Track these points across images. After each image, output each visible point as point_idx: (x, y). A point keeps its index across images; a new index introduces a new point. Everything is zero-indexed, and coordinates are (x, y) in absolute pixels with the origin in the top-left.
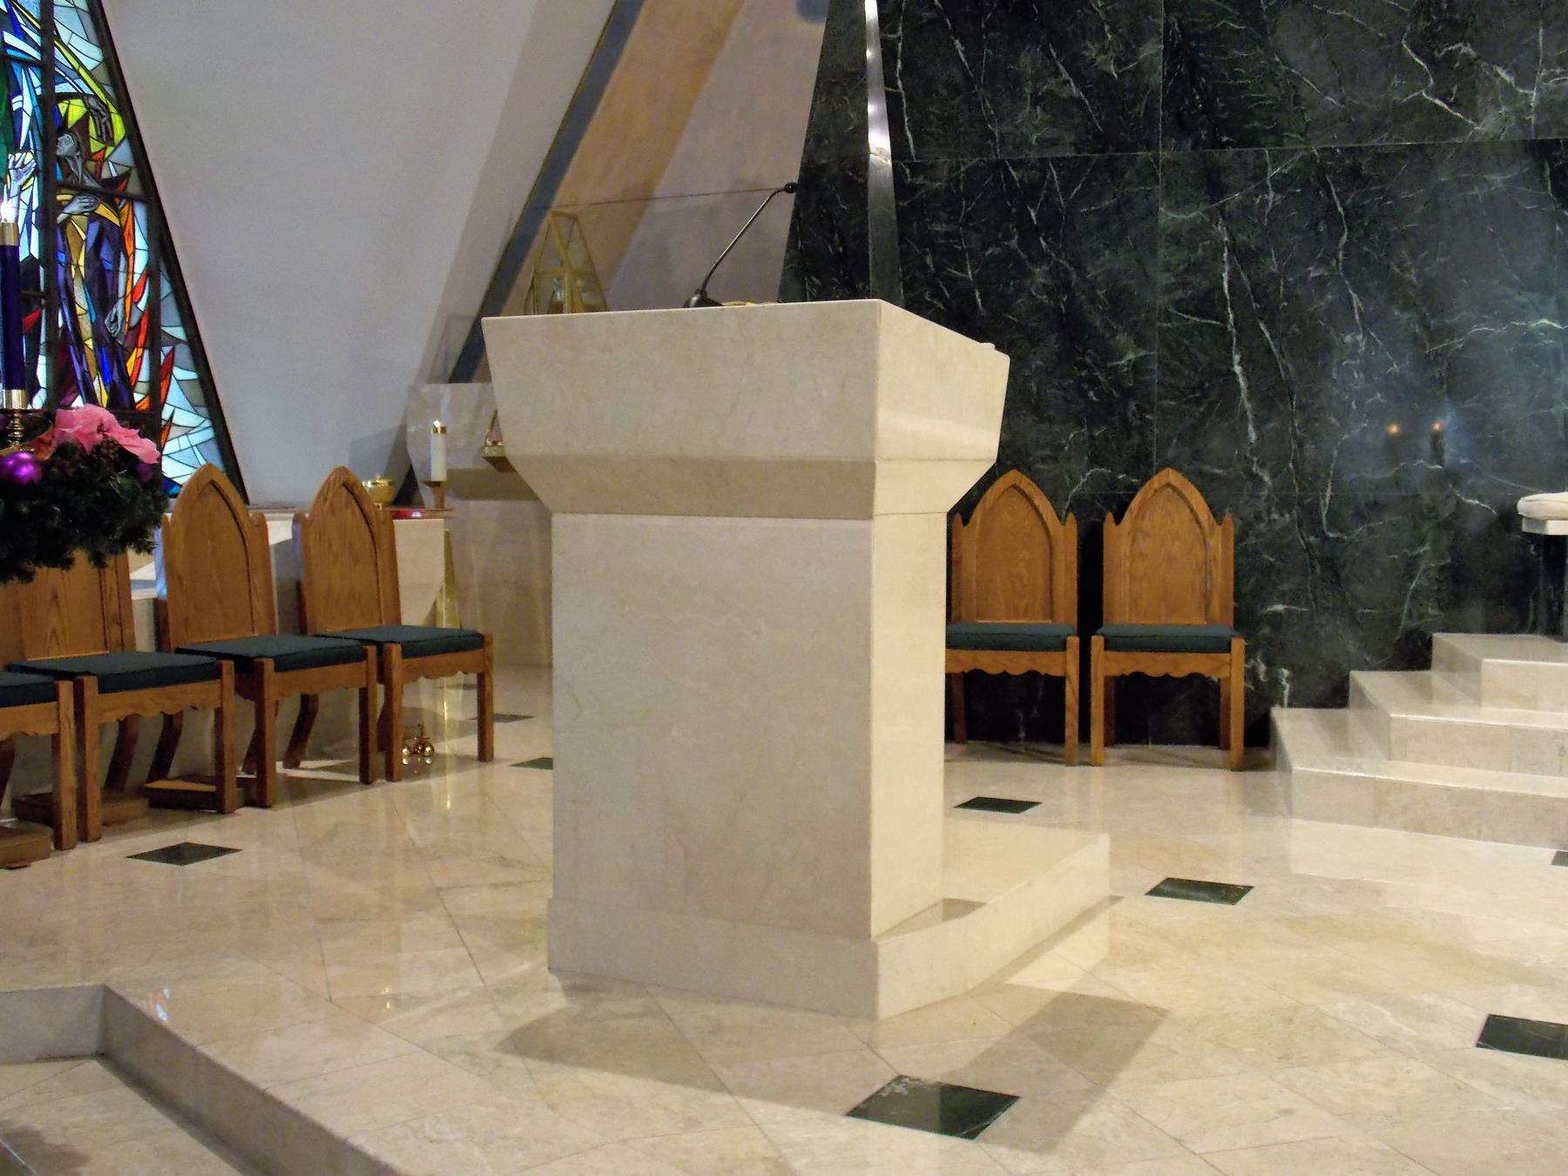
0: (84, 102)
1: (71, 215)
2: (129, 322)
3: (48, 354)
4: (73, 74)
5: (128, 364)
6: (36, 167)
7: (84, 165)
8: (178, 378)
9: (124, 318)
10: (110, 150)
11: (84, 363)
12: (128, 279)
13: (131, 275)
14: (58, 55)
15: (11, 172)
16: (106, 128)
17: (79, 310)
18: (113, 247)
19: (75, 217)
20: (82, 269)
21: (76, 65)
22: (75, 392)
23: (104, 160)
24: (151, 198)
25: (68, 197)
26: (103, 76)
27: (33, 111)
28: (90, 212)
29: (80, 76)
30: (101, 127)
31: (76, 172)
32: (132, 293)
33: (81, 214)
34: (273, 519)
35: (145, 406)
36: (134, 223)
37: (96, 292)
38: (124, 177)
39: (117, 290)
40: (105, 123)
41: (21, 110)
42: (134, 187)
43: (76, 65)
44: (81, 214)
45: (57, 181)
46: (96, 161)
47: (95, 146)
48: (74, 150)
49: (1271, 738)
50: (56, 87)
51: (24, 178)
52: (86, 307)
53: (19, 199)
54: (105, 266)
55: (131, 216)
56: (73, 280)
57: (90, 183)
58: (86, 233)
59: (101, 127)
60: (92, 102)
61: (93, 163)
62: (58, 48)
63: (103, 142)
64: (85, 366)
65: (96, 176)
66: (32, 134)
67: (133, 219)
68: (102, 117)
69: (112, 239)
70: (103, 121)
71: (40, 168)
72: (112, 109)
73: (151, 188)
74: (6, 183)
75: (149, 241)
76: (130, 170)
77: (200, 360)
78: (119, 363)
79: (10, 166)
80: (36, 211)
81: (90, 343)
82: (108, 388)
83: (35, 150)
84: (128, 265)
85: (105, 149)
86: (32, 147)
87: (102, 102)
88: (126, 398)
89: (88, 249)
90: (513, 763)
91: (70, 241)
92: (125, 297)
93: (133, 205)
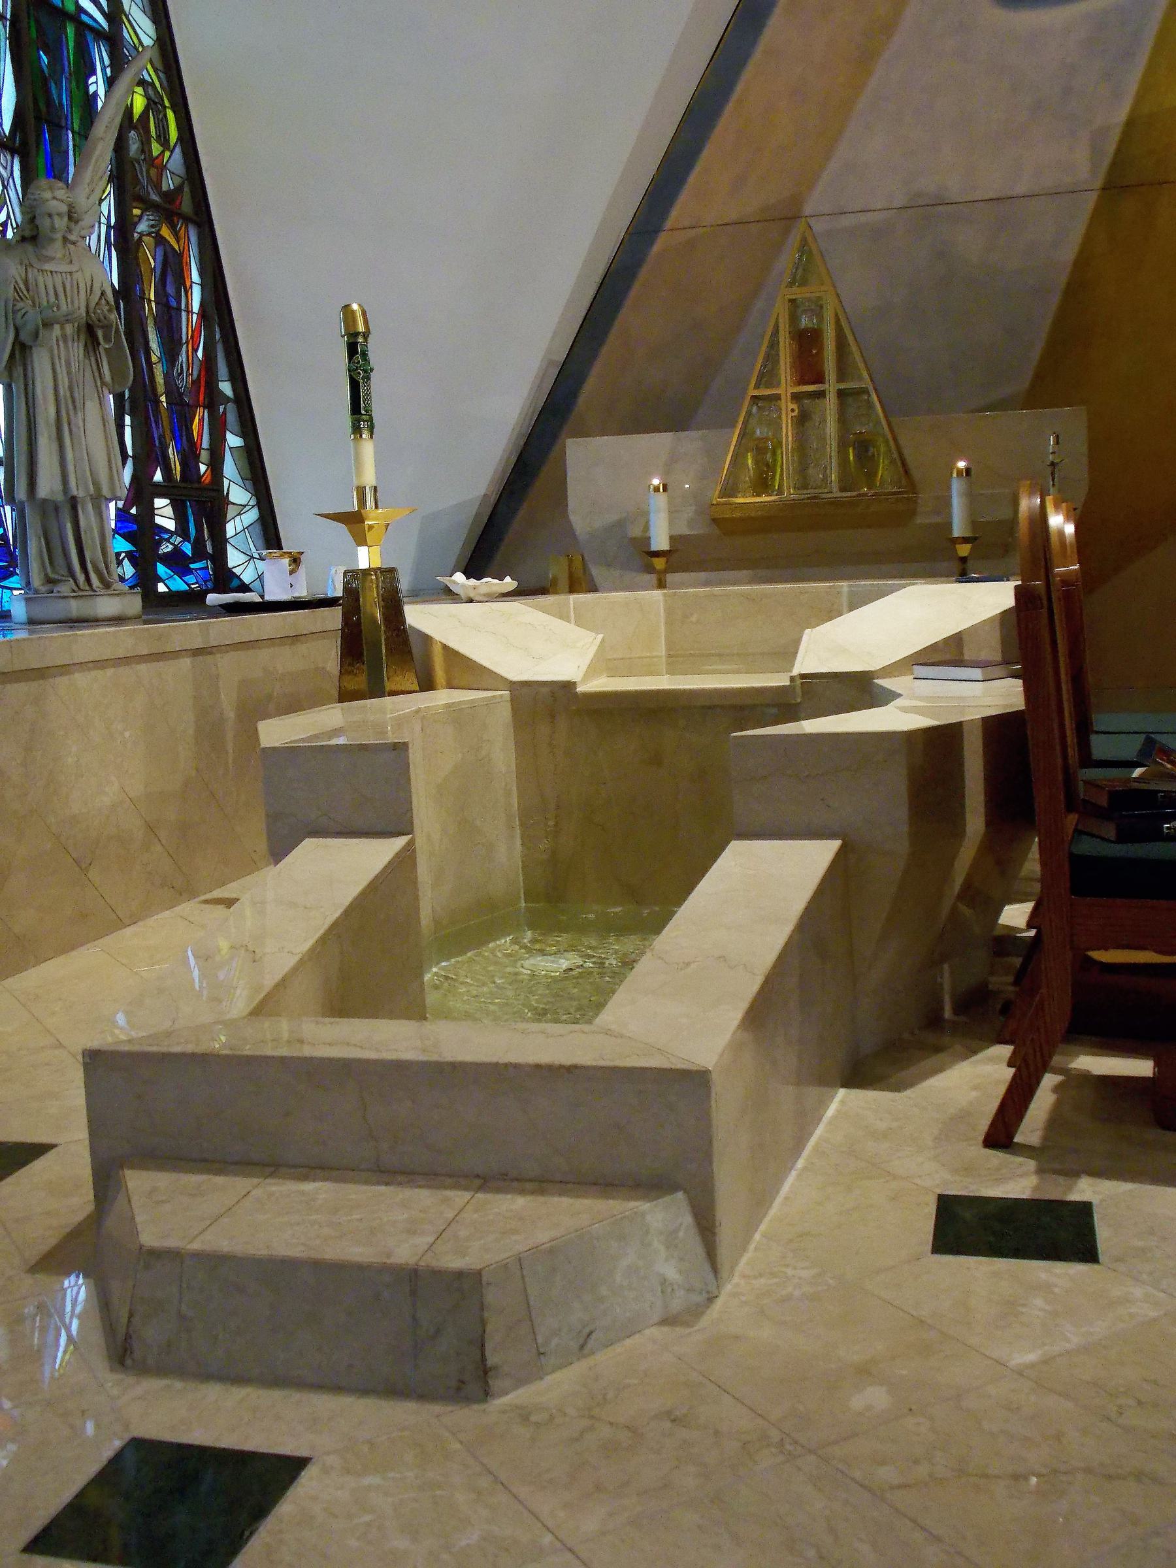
2: (192, 375)
8: (232, 445)
10: (167, 154)
16: (163, 127)
17: (154, 359)
24: (203, 219)
31: (142, 181)
32: (192, 337)
33: (149, 234)
34: (409, 603)
35: (207, 479)
38: (179, 189)
41: (96, 94)
42: (186, 206)
44: (149, 234)
47: (156, 149)
49: (1096, 1050)
52: (158, 355)
55: (186, 239)
64: (161, 430)
69: (173, 267)
73: (248, 416)
75: (201, 274)
77: (249, 429)
82: (180, 456)
90: (711, 1276)
92: (187, 342)
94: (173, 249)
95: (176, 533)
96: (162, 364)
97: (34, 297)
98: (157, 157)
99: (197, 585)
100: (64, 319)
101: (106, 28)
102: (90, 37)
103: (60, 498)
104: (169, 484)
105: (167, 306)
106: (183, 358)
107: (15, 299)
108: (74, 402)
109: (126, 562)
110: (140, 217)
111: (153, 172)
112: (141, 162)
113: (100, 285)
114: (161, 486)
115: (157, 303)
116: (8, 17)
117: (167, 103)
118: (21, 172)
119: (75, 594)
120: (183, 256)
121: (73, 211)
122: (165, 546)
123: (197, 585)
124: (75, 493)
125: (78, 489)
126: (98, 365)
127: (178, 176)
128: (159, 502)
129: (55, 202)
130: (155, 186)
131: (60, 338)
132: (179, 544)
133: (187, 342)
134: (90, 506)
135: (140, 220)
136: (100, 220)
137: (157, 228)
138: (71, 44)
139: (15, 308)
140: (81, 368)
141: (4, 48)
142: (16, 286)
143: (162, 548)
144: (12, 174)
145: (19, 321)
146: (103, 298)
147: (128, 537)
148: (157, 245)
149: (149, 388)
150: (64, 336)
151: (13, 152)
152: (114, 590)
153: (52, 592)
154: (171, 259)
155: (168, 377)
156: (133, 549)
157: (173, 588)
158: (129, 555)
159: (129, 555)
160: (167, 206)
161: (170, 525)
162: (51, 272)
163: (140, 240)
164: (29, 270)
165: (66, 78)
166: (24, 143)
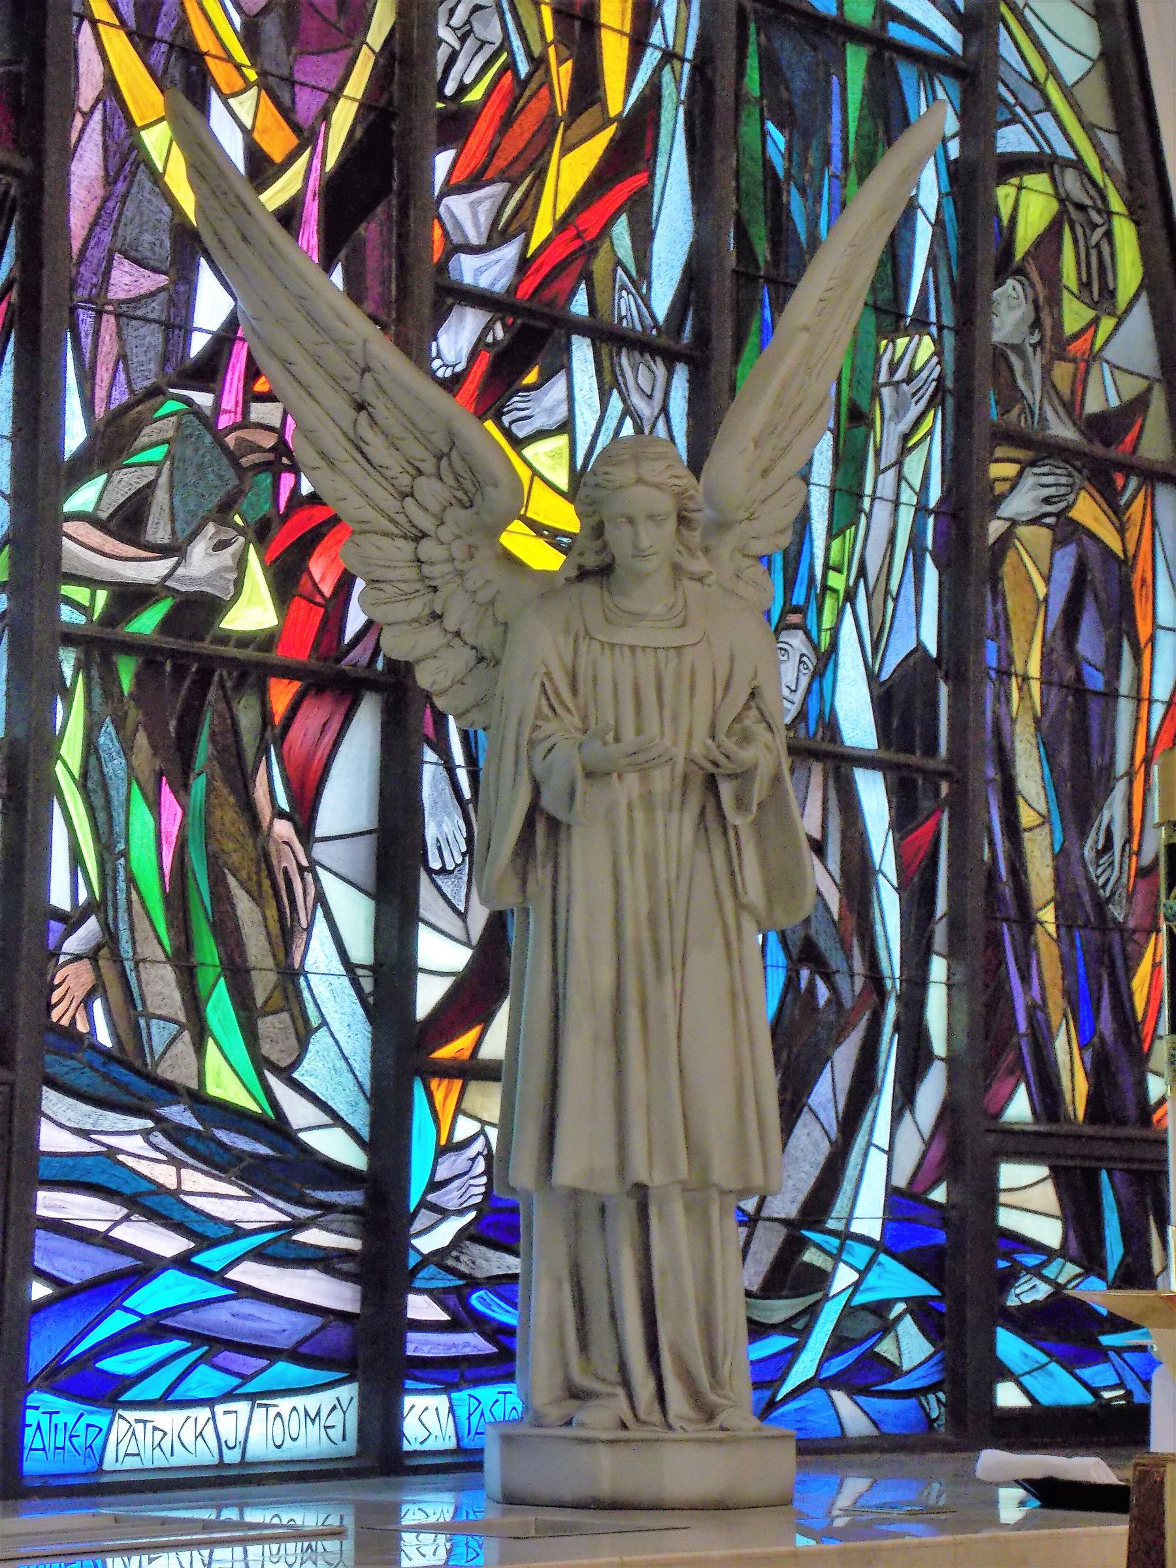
0: (1053, 179)
1: (1014, 523)
3: (952, 955)
4: (1033, 99)
5: (1136, 983)
6: (940, 379)
7: (1047, 370)
9: (1128, 841)
10: (1107, 324)
11: (1034, 972)
12: (1137, 719)
13: (1145, 705)
14: (1006, 48)
15: (886, 392)
17: (1027, 817)
18: (1105, 621)
19: (1022, 531)
20: (1035, 687)
21: (1040, 70)
22: (1011, 1072)
23: (1093, 357)
25: (1010, 470)
26: (1099, 110)
27: (940, 206)
28: (1057, 515)
29: (1048, 106)
30: (1088, 255)
31: (1028, 394)
33: (1036, 521)
36: (1153, 539)
37: (1064, 759)
38: (1137, 406)
39: (1112, 757)
40: (1097, 246)
43: (1040, 70)
44: (1036, 521)
45: (992, 421)
46: (1074, 360)
47: (1074, 315)
48: (1026, 329)
50: (260, 1022)
51: (914, 411)
53: (900, 477)
54: (1086, 678)
55: (1148, 519)
56: (1013, 721)
57: (1062, 430)
58: (1047, 580)
59: (1088, 255)
60: (1071, 182)
61: (1069, 367)
62: (1008, 28)
63: (1093, 305)
64: (1036, 992)
65: (1071, 407)
66: (935, 276)
67: (1153, 539)
68: (1095, 226)
70: (1094, 239)
71: (949, 383)
72: (1116, 204)
74: (871, 426)
76: (1149, 390)
78: (1112, 974)
79: (883, 378)
80: (936, 512)
81: (1048, 915)
82: (1088, 1055)
83: (941, 328)
84: (1138, 679)
85: (1095, 322)
86: (933, 318)
87: (1094, 183)
88: (1131, 1097)
89: (1051, 626)
91: (1009, 603)
92: (1130, 775)
93: (1153, 488)
94: (1107, 551)
95: (1063, 1253)
96: (1052, 833)
97: (586, 707)
98: (1077, 336)
99: (1121, 1392)
100: (628, 761)
101: (958, 48)
102: (907, 73)
103: (608, 1185)
104: (1053, 1128)
105: (1079, 690)
106: (1114, 811)
107: (539, 715)
108: (658, 955)
109: (908, 1328)
110: (1015, 483)
111: (1062, 373)
112: (1030, 350)
113: (750, 674)
114: (1025, 1133)
115: (1046, 682)
116: (689, 55)
117: (1116, 204)
118: (691, 401)
119: (623, 1434)
120: (1133, 567)
121: (691, 505)
122: (1026, 1287)
123: (1121, 1392)
124: (642, 1176)
125: (651, 1167)
126: (730, 862)
127: (1139, 375)
128: (1012, 1174)
129: (640, 490)
130: (1064, 405)
131: (637, 803)
132: (1069, 1282)
133: (1130, 775)
134: (678, 1208)
135: (1012, 488)
136: (898, 495)
137: (1063, 505)
138: (855, 96)
139: (540, 734)
140: (685, 875)
141: (671, 125)
142: (547, 684)
143: (1018, 1291)
144: (665, 409)
145: (539, 770)
146: (753, 704)
147: (915, 1263)
148: (1058, 543)
149: (1008, 892)
150: (648, 798)
151: (671, 359)
152: (722, 1429)
153: (569, 1423)
154: (1096, 574)
155: (1062, 859)
156: (931, 1291)
157: (1046, 1399)
158: (919, 1309)
159: (919, 1309)
160: (1098, 449)
161: (1050, 1232)
162: (633, 648)
163: (1006, 539)
164: (583, 647)
165: (833, 176)
166: (703, 337)
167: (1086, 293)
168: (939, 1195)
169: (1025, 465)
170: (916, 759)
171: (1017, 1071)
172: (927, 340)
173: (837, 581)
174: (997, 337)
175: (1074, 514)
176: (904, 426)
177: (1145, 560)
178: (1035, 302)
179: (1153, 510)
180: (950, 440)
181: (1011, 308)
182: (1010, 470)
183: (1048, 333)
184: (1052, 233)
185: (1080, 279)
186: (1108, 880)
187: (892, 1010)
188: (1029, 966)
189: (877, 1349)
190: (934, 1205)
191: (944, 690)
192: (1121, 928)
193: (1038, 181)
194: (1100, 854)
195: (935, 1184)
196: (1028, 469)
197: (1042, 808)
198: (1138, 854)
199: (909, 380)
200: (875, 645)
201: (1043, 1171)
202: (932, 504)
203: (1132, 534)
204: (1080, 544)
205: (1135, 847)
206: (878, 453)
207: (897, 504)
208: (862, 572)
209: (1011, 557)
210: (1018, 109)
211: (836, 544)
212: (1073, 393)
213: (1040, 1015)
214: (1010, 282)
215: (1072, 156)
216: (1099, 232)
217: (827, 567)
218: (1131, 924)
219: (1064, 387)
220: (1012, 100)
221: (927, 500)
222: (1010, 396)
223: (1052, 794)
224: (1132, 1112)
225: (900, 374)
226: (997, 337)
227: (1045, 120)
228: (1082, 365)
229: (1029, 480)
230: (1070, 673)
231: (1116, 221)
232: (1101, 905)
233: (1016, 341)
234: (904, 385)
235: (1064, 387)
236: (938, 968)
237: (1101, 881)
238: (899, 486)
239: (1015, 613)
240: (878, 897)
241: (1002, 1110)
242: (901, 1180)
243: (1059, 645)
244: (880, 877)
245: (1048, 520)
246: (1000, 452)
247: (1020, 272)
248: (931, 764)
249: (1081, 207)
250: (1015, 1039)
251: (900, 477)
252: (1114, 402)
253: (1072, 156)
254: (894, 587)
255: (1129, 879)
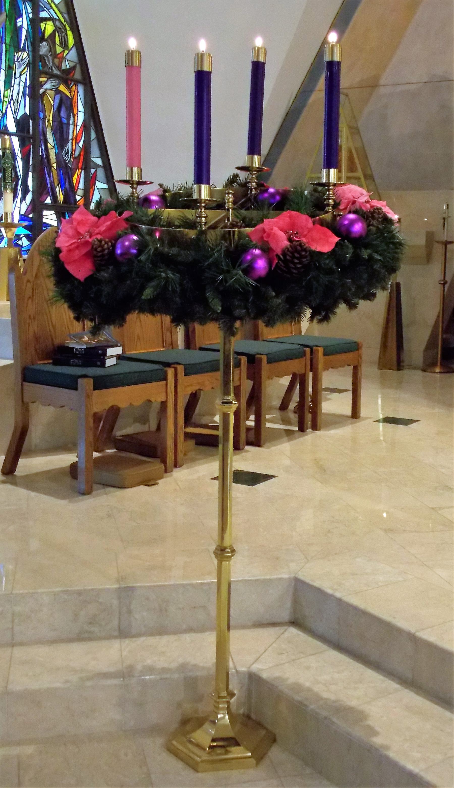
1: (46, 90)
3: (33, 172)
4: (48, 7)
5: (74, 179)
7: (53, 60)
9: (72, 152)
10: (66, 52)
15: (16, 63)
17: (50, 147)
18: (67, 109)
19: (48, 91)
20: (51, 122)
22: (46, 194)
25: (45, 79)
26: (63, 9)
29: (52, 8)
33: (51, 90)
36: (77, 95)
40: (64, 36)
44: (51, 90)
47: (59, 50)
48: (48, 52)
53: (20, 80)
57: (56, 72)
58: (54, 101)
60: (58, 23)
65: (59, 68)
68: (63, 32)
71: (31, 62)
72: (68, 28)
76: (76, 65)
79: (16, 60)
81: (54, 165)
82: (63, 192)
85: (64, 51)
89: (55, 110)
92: (73, 139)
94: (67, 96)
98: (59, 54)
105: (61, 122)
109: (24, 239)
110: (46, 82)
111: (56, 61)
117: (68, 28)
148: (56, 94)
154: (64, 100)
158: (27, 236)
163: (44, 93)
167: (61, 45)
168: (31, 216)
169: (48, 79)
170: (25, 134)
171: (48, 194)
172: (25, 53)
173: (6, 100)
174: (41, 53)
175: (59, 88)
176: (21, 70)
177: (76, 98)
178: (50, 47)
179: (77, 88)
180: (31, 73)
181: (45, 48)
182: (45, 79)
183: (53, 53)
184: (54, 32)
185: (60, 43)
186: (68, 159)
187: (20, 182)
188: (50, 175)
189: (18, 243)
190: (30, 218)
191: (31, 121)
192: (70, 168)
193: (50, 23)
194: (66, 154)
195: (30, 214)
196: (49, 80)
197: (53, 145)
198: (75, 154)
199: (22, 60)
200: (15, 113)
201: (54, 212)
202: (27, 86)
203: (73, 93)
204: (61, 95)
205: (74, 153)
206: (15, 75)
207: (19, 85)
208: (12, 98)
209: (45, 97)
210: (45, 8)
211: (6, 92)
212: (59, 65)
213: (53, 184)
214: (44, 43)
215: (58, 18)
216: (63, 34)
217: (4, 97)
218: (73, 167)
219: (57, 64)
220: (43, 6)
221: (26, 85)
222: (44, 65)
223: (55, 142)
224: (73, 202)
225: (20, 59)
226: (41, 53)
227: (51, 11)
228: (61, 59)
229: (49, 82)
230: (59, 119)
231: (68, 31)
232: (66, 164)
233: (46, 54)
234: (21, 62)
235: (57, 64)
236: (30, 174)
237: (66, 159)
238: (20, 82)
239: (47, 107)
240: (17, 161)
241: (44, 201)
242: (23, 212)
243: (57, 114)
244: (17, 157)
245: (54, 90)
246: (43, 76)
247: (46, 41)
248: (28, 136)
249: (60, 28)
250: (47, 188)
251: (20, 80)
252: (68, 67)
253: (58, 18)
254: (19, 101)
255: (72, 159)
